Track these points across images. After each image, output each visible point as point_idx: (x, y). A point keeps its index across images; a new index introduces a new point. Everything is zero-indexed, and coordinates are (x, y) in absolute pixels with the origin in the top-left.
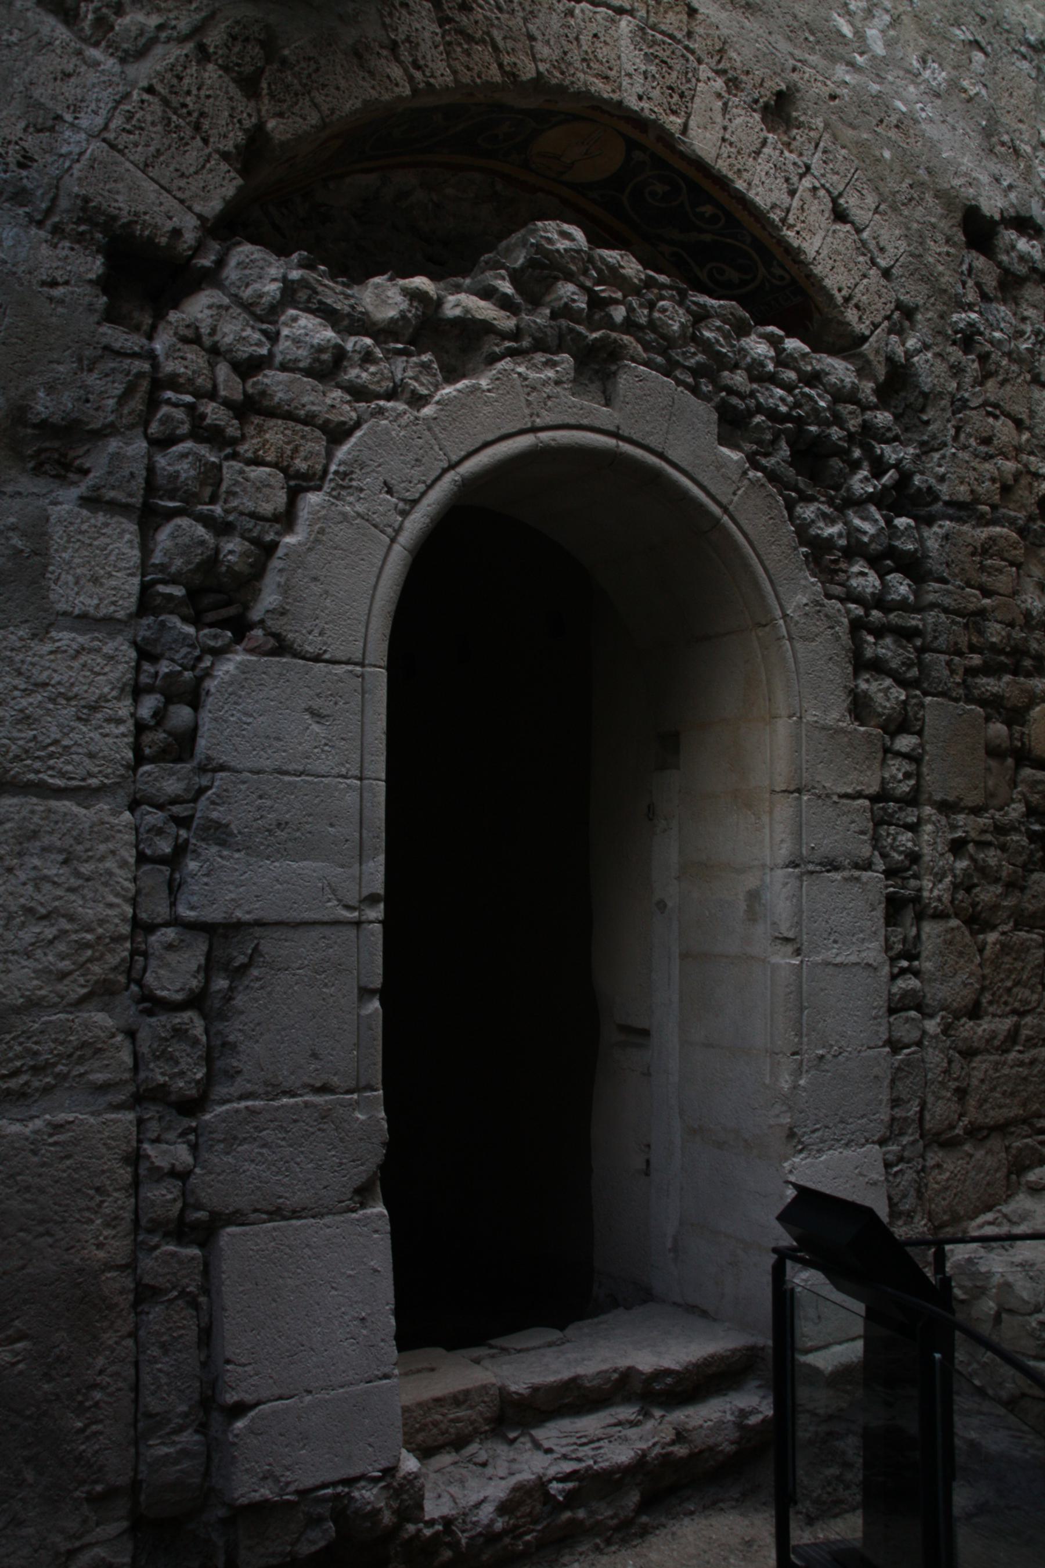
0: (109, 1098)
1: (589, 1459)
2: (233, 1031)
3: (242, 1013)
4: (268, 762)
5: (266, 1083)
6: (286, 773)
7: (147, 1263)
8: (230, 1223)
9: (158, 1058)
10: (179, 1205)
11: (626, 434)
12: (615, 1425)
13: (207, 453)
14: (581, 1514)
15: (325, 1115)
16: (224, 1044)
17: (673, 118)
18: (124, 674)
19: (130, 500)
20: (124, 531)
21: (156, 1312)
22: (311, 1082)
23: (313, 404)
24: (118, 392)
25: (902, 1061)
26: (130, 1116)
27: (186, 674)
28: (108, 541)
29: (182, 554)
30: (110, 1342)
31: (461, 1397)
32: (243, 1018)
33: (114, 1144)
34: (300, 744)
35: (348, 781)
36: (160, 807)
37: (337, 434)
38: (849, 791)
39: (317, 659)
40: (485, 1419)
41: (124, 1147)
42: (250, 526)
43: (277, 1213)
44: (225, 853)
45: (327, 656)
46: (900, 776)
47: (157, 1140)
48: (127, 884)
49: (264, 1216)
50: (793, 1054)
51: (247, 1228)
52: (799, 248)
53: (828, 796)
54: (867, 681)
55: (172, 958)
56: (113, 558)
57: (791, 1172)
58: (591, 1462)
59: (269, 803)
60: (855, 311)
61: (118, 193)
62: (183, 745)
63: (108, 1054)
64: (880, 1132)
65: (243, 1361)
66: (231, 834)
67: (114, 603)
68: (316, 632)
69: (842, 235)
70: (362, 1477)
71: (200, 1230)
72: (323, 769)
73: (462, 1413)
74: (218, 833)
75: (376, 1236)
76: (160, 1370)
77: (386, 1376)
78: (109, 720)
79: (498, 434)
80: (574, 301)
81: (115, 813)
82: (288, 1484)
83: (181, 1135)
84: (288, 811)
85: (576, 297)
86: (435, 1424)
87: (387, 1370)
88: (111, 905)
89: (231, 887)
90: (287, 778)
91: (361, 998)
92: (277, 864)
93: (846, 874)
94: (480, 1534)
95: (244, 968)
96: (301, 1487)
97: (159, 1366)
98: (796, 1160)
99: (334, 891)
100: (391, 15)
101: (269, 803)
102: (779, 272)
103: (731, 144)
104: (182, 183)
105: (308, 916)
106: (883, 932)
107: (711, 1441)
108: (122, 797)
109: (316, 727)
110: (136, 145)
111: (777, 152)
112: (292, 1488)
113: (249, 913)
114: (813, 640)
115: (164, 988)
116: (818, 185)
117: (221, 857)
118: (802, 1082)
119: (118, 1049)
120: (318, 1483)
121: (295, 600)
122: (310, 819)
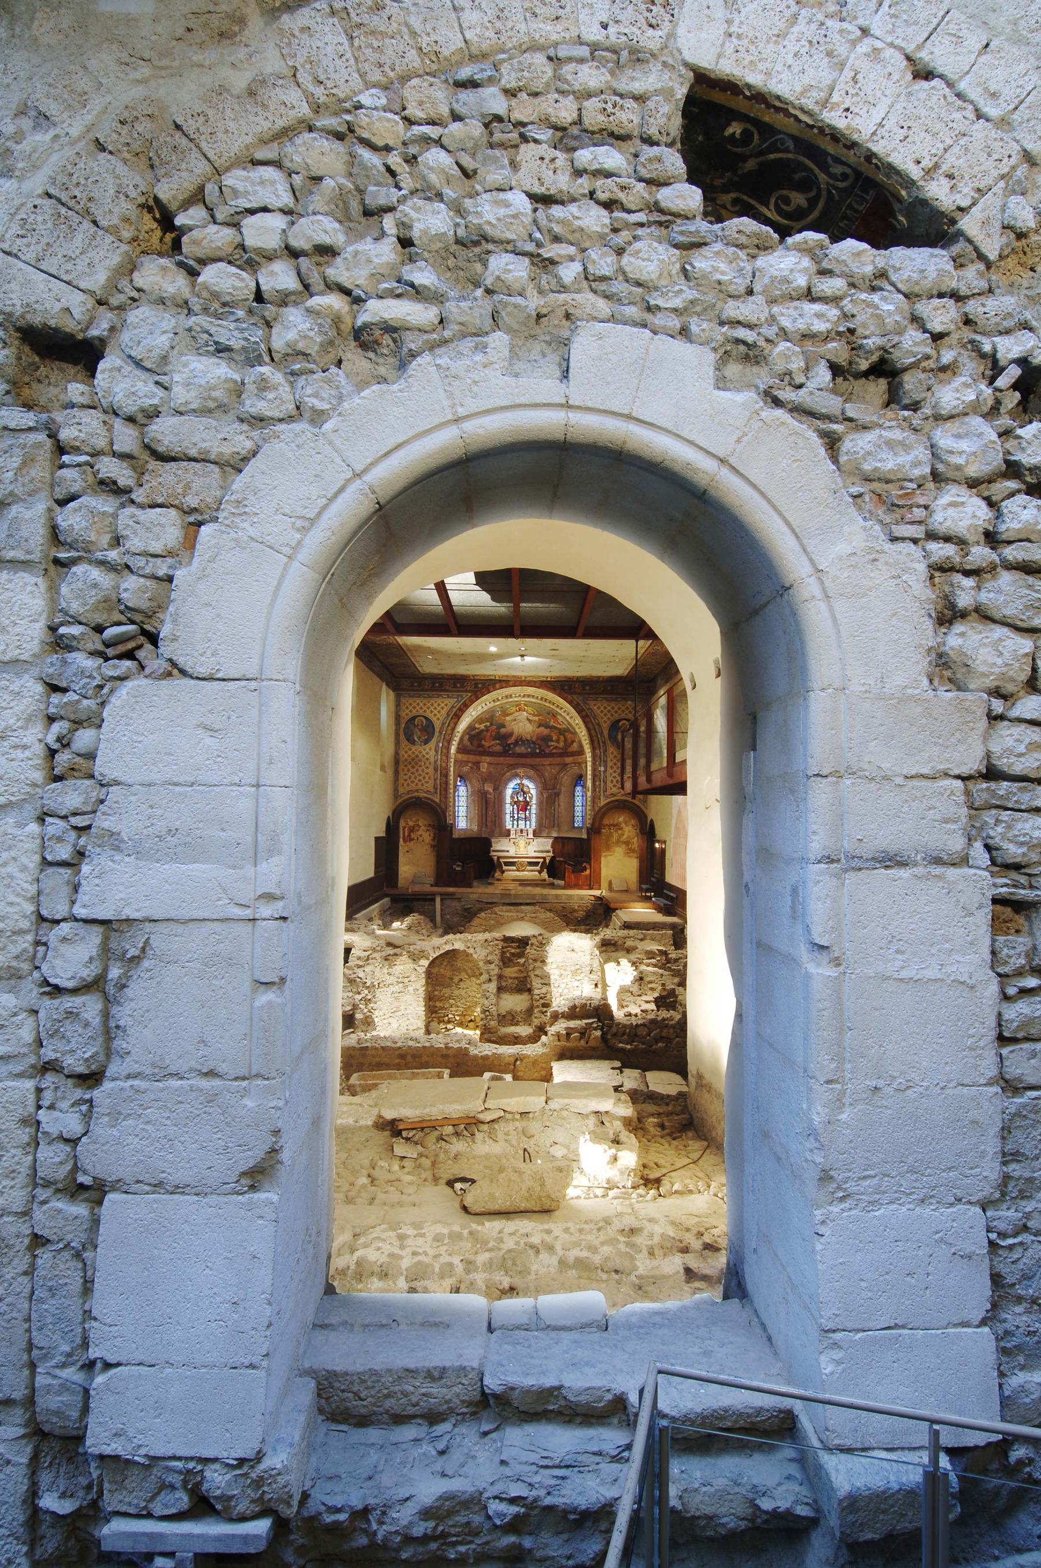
0: (10, 1067)
1: (541, 1488)
2: (123, 1015)
3: (132, 1000)
4: (159, 776)
5: (153, 1065)
6: (176, 784)
7: (38, 1214)
8: (114, 1189)
9: (52, 1036)
10: (68, 1167)
11: (577, 404)
12: (594, 1454)
13: (105, 504)
14: (527, 1542)
15: (211, 1099)
16: (118, 1027)
17: (650, 32)
18: (28, 707)
19: (28, 557)
20: (26, 584)
21: (45, 1256)
22: (199, 1067)
23: (204, 441)
24: (16, 465)
25: (1024, 1106)
26: (29, 1084)
27: (85, 702)
28: (12, 594)
29: (78, 597)
30: (8, 1277)
31: (436, 1374)
32: (133, 1004)
33: (12, 1107)
34: (192, 757)
35: (241, 789)
36: (65, 817)
37: (236, 465)
38: (925, 771)
39: (211, 678)
40: (463, 1402)
41: (20, 1111)
42: (142, 564)
43: (158, 1186)
44: (117, 858)
45: (219, 675)
46: (1022, 749)
47: (51, 1107)
48: (26, 886)
49: (147, 1188)
50: (828, 1082)
51: (130, 1196)
52: (848, 127)
53: (886, 778)
54: (962, 634)
55: (64, 948)
56: (16, 608)
57: (823, 1222)
58: (542, 1493)
59: (159, 812)
60: (944, 181)
61: (12, 292)
62: (85, 766)
63: (8, 1030)
64: (987, 1190)
65: (108, 1321)
66: (122, 841)
67: (18, 647)
68: (209, 653)
69: (923, 95)
70: (215, 1460)
71: (93, 1192)
72: (214, 779)
73: (435, 1389)
74: (113, 841)
75: (260, 1222)
76: (46, 1310)
77: (252, 1366)
78: (15, 747)
79: (411, 433)
80: (510, 271)
81: (21, 825)
82: (140, 1446)
83: (73, 1105)
84: (178, 819)
85: (511, 267)
86: (405, 1394)
87: (255, 1360)
88: (11, 904)
89: (121, 888)
90: (178, 789)
91: (254, 991)
92: (166, 867)
93: (920, 870)
94: (397, 1532)
95: (136, 960)
96: (152, 1453)
97: (45, 1307)
98: (835, 1209)
99: (225, 891)
100: (289, 44)
101: (159, 812)
102: (838, 170)
103: (739, 37)
104: (69, 266)
105: (196, 914)
106: (988, 942)
107: (709, 1510)
108: (30, 811)
109: (209, 741)
110: (28, 245)
111: (814, 26)
112: (143, 1451)
113: (138, 910)
114: (865, 595)
115: (56, 976)
116: (879, 44)
117: (113, 861)
118: (844, 1117)
119: (19, 1027)
120: (170, 1454)
121: (186, 626)
122: (201, 825)
